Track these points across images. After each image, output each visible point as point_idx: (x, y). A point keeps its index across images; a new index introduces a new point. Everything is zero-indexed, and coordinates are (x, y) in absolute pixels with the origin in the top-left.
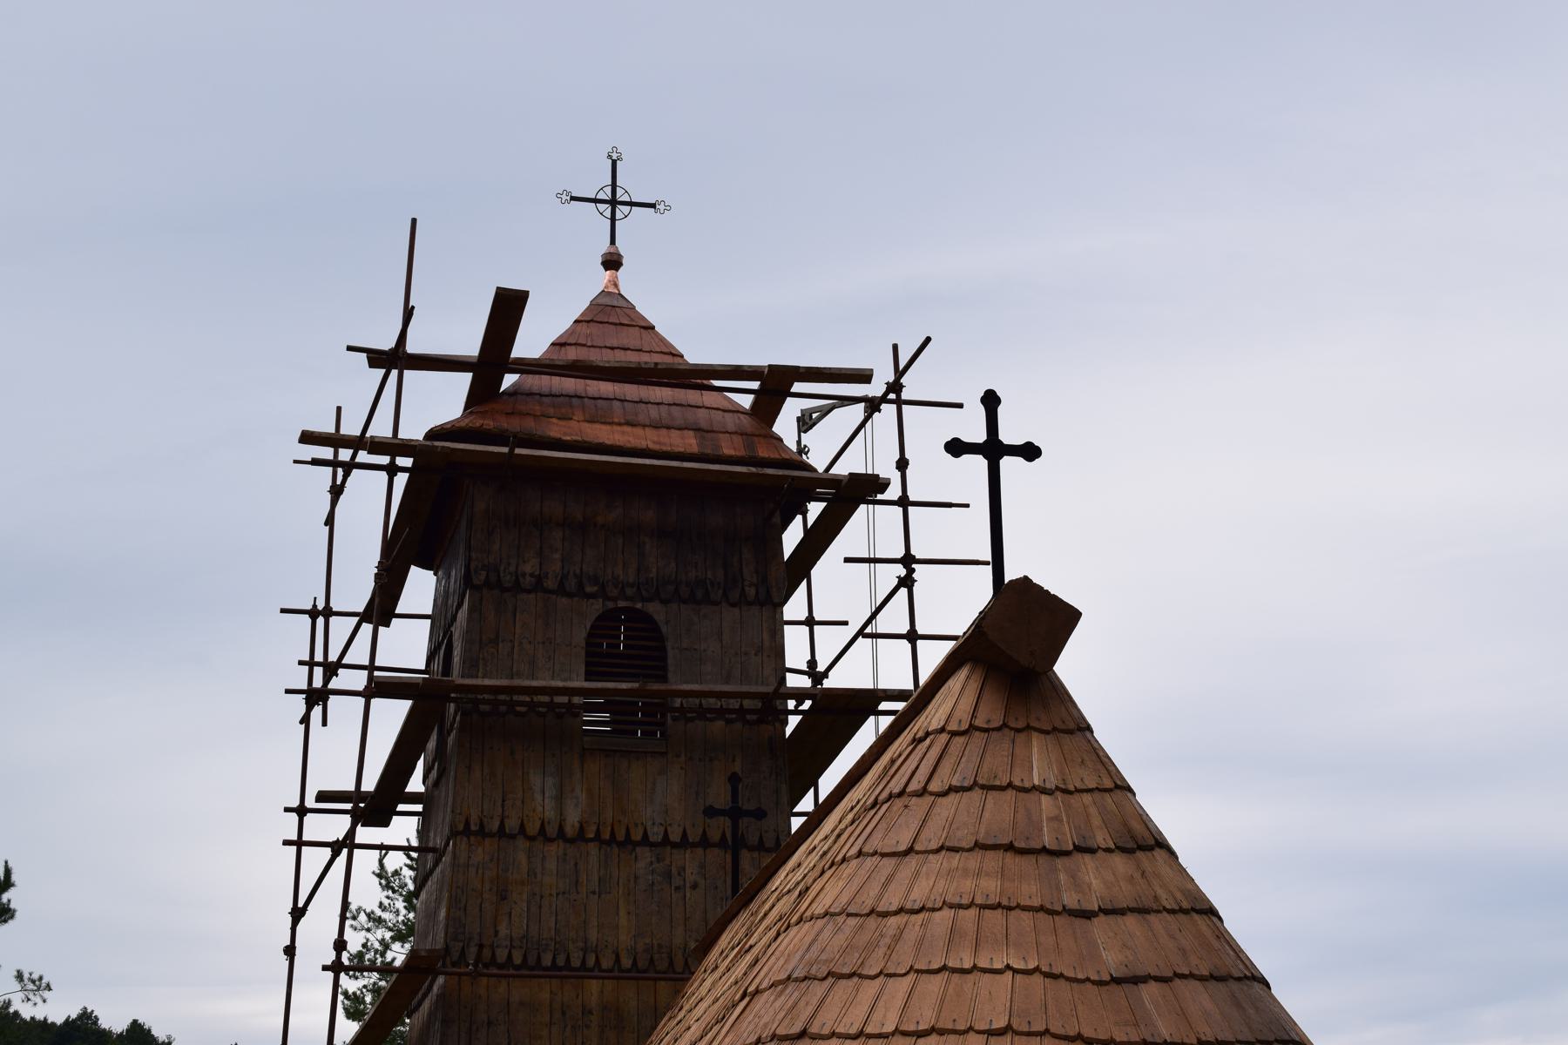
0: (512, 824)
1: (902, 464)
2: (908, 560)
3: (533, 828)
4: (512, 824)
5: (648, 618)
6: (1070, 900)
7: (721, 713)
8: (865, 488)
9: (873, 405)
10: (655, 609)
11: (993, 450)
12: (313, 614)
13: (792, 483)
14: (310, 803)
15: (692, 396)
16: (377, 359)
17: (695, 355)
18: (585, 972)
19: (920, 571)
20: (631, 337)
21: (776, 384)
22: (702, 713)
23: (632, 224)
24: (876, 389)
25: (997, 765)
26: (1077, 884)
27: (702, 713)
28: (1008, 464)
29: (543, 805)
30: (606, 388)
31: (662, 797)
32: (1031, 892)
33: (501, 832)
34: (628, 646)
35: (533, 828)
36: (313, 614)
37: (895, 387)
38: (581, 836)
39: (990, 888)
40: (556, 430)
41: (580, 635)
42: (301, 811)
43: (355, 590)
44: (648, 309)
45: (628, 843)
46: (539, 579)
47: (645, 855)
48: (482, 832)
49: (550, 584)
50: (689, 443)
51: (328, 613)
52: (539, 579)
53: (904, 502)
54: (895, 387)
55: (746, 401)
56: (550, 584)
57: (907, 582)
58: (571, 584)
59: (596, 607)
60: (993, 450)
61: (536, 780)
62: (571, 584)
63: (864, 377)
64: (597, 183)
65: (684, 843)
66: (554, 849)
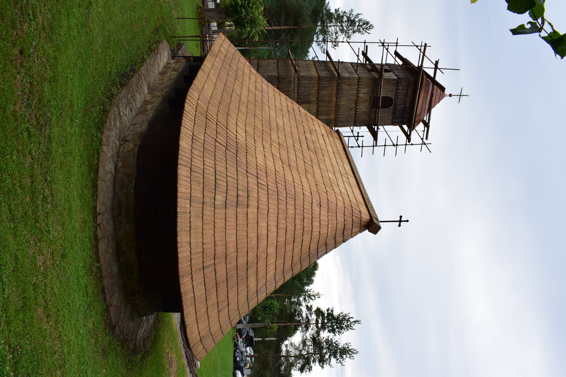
0: (360, 86)
1: (412, 144)
2: (397, 145)
3: (359, 89)
4: (360, 86)
5: (391, 105)
6: (337, 236)
7: (375, 117)
8: (408, 137)
9: (422, 139)
10: (393, 106)
11: (400, 221)
12: (397, 43)
13: (412, 127)
14: (366, 44)
15: (426, 111)
16: (437, 62)
17: (433, 110)
18: (337, 97)
19: (394, 148)
20: (437, 100)
21: (427, 125)
22: (375, 114)
23: (457, 98)
24: (425, 140)
25: (355, 225)
26: (339, 237)
27: (375, 114)
28: (398, 223)
29: (363, 91)
30: (429, 98)
31: (363, 108)
32: (338, 232)
33: (359, 84)
34: (387, 102)
35: (359, 89)
36: (397, 43)
37: (424, 144)
38: (358, 96)
39: (339, 227)
40: (422, 92)
41: (389, 95)
42: (365, 43)
43: (400, 51)
44: (442, 101)
45: (356, 103)
46: (398, 89)
47: (354, 106)
48: (359, 82)
49: (398, 91)
50: (418, 112)
51: (397, 46)
52: (398, 89)
53: (406, 145)
54: (424, 144)
55: (425, 119)
56: (398, 91)
57: (394, 145)
58: (397, 94)
59: (393, 98)
60: (400, 221)
61: (367, 89)
62: (397, 94)
63: (427, 139)
64: (464, 93)
65: (356, 111)
66: (356, 92)
